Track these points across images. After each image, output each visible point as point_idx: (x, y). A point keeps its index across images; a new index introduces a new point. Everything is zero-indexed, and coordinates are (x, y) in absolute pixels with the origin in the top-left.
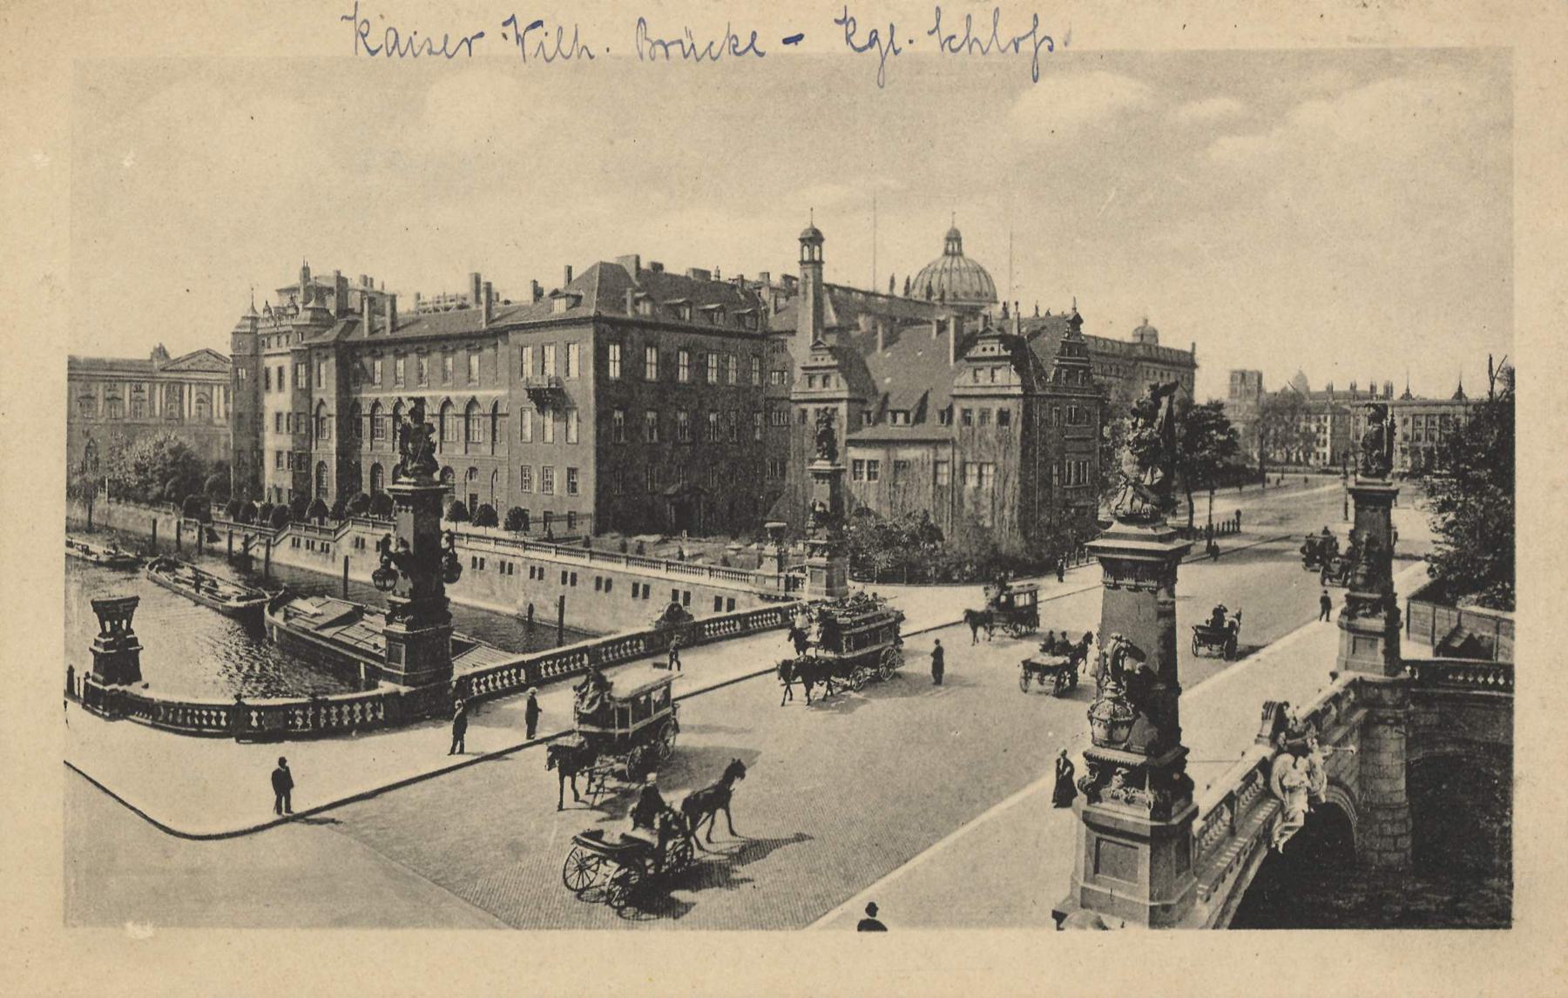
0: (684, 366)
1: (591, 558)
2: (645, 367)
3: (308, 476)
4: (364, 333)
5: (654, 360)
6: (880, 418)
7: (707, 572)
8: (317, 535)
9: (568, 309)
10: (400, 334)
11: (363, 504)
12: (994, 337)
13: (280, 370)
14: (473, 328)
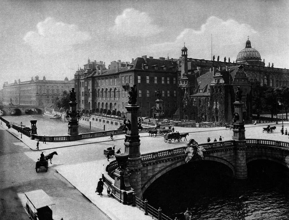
0: (156, 80)
1: (149, 125)
2: (138, 80)
3: (87, 104)
4: (97, 74)
5: (140, 78)
6: (197, 92)
7: (148, 124)
8: (87, 117)
9: (130, 68)
10: (104, 74)
11: (97, 111)
12: (219, 72)
13: (83, 82)
14: (116, 73)
